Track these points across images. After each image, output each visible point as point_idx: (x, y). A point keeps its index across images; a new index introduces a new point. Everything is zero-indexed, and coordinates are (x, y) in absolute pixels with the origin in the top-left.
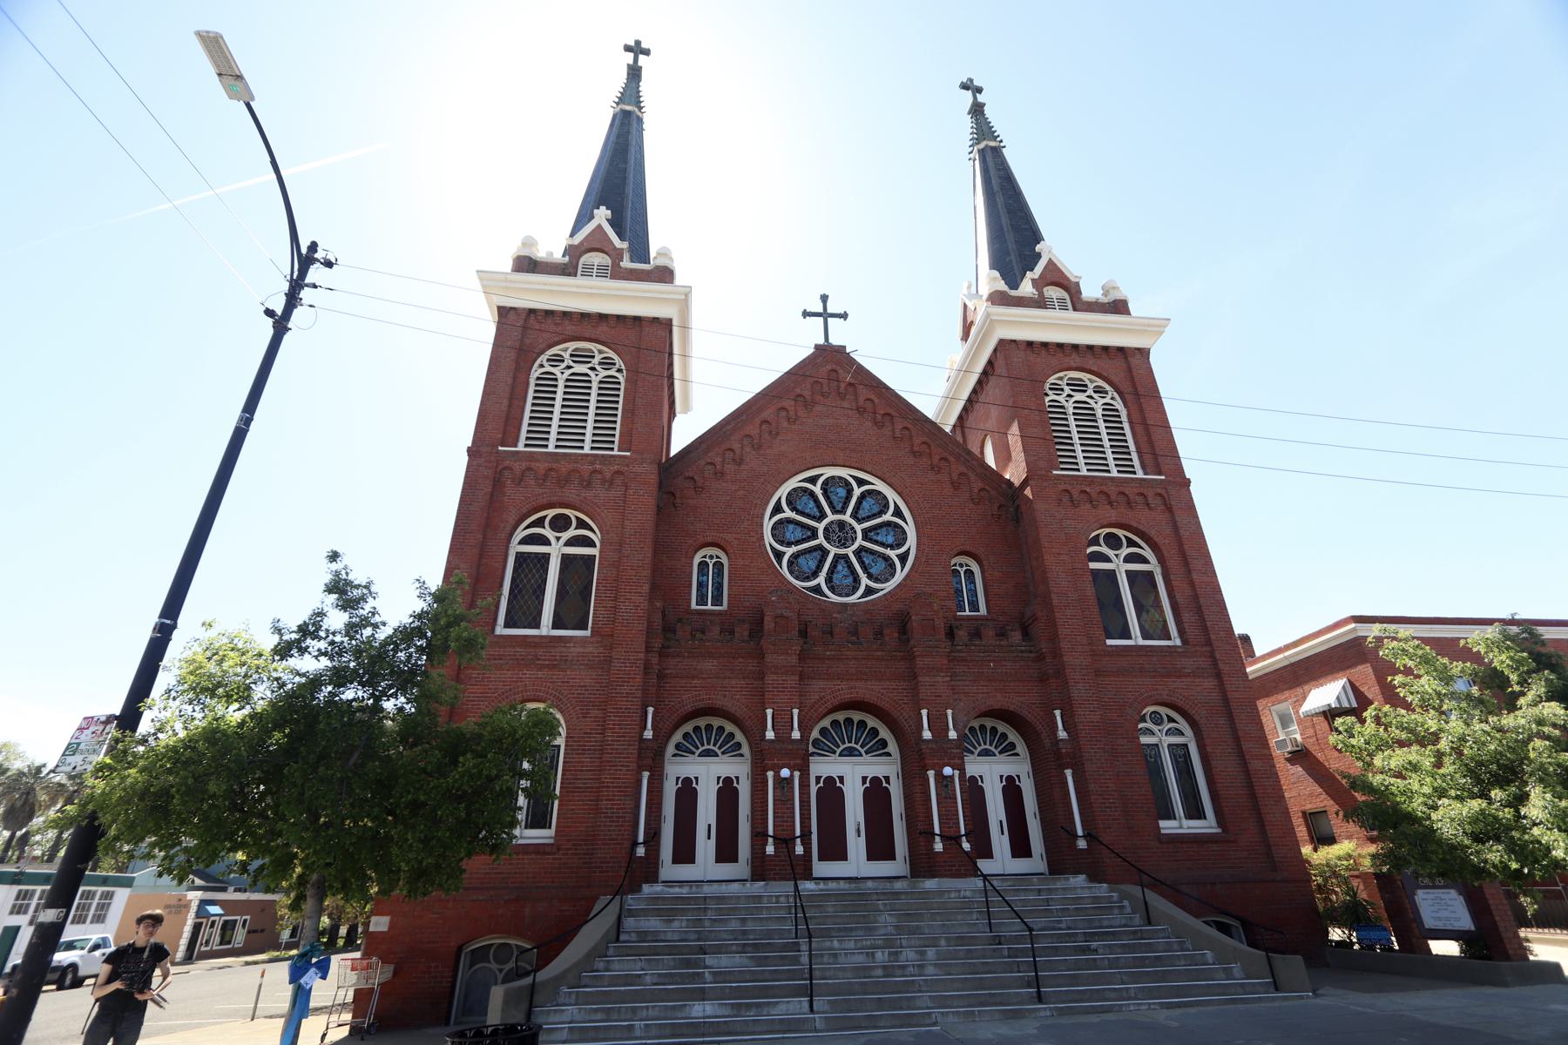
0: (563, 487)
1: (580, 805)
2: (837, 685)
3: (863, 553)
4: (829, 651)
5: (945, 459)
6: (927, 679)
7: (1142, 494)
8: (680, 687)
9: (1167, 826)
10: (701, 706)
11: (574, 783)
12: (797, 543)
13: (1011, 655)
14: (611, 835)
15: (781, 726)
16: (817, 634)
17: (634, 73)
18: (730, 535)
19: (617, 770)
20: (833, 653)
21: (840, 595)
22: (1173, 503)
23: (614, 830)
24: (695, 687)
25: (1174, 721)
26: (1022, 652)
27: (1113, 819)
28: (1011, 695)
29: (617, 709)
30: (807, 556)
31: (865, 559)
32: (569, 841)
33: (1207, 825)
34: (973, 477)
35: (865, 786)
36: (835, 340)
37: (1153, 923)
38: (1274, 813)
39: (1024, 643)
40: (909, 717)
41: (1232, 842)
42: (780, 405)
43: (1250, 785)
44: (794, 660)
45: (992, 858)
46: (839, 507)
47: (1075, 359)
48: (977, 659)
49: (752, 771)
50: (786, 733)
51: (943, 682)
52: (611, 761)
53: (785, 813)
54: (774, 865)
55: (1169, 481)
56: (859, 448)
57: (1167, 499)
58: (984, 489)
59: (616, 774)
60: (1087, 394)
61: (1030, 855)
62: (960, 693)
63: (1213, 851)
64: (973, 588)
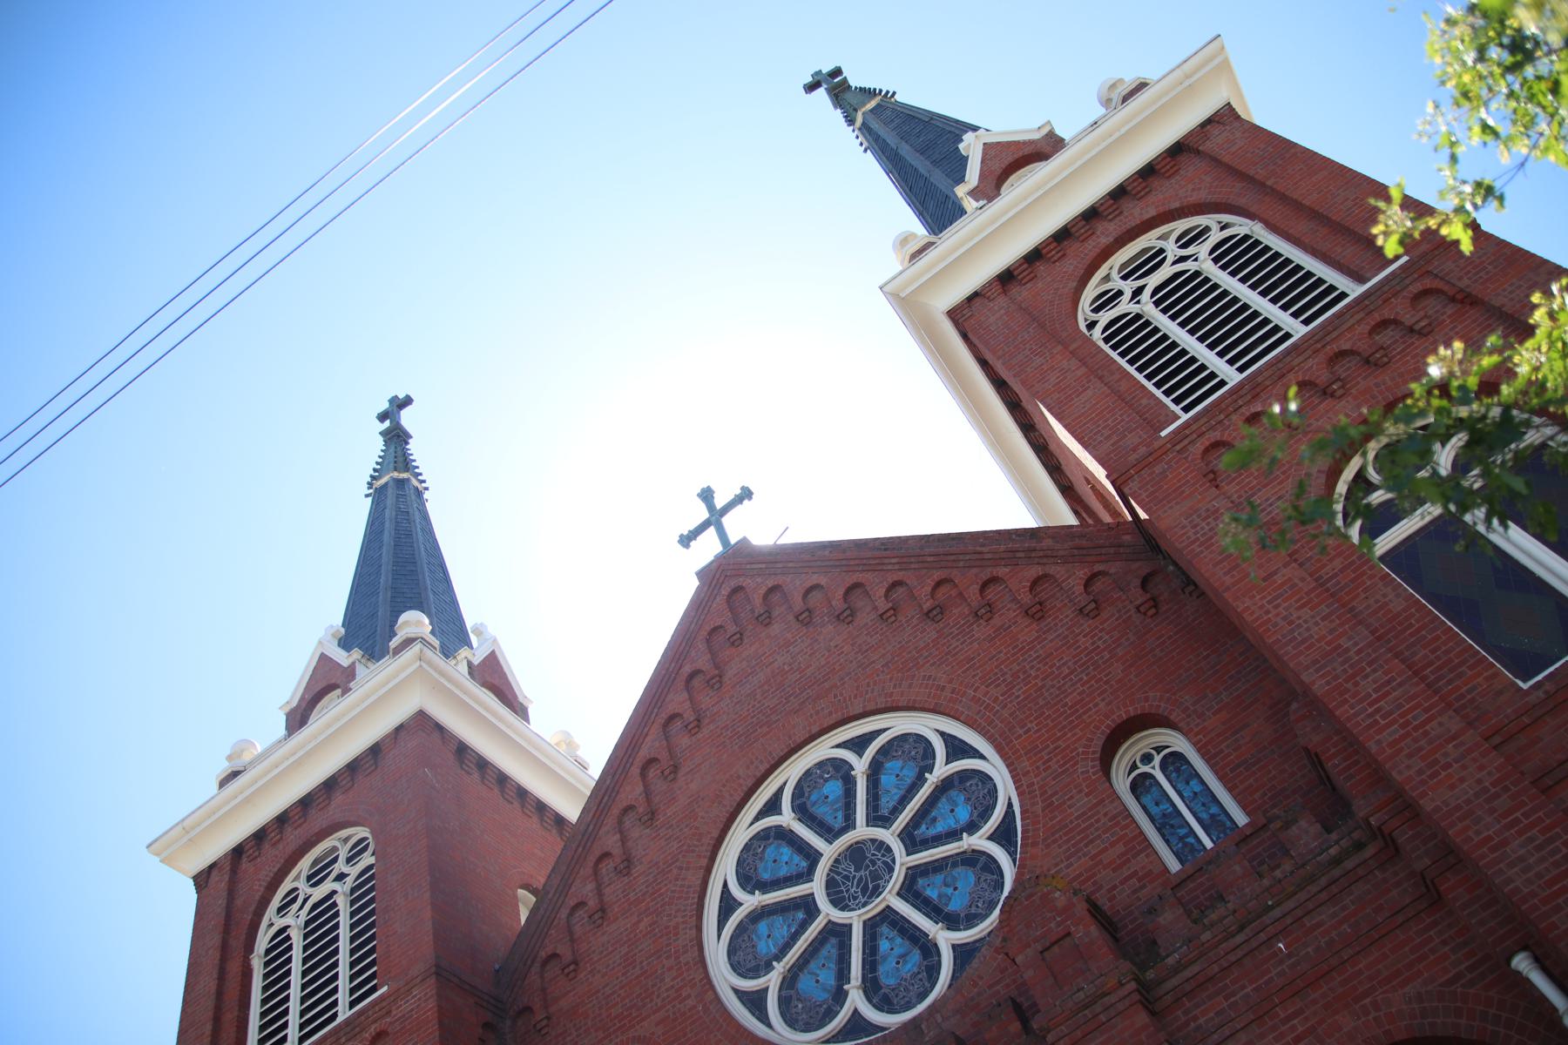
3: (921, 881)
5: (993, 580)
7: (1384, 324)
12: (843, 975)
13: (1313, 889)
17: (396, 438)
18: (645, 1024)
22: (1461, 284)
34: (1056, 570)
39: (1334, 836)
42: (664, 716)
46: (838, 823)
47: (1106, 231)
48: (1232, 958)
55: (1424, 255)
56: (827, 685)
57: (1446, 288)
64: (1198, 788)
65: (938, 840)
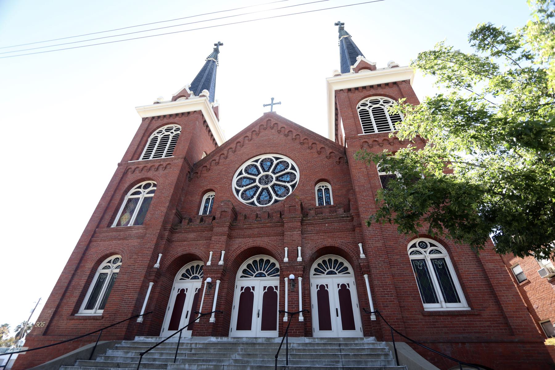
0: (148, 172)
1: (117, 297)
2: (248, 240)
3: (275, 186)
4: (245, 225)
6: (289, 233)
8: (178, 245)
9: (429, 307)
10: (185, 253)
11: (118, 287)
12: (254, 194)
14: (124, 311)
15: (215, 259)
16: (242, 218)
17: (216, 51)
19: (135, 281)
20: (247, 226)
21: (263, 204)
23: (126, 309)
24: (185, 245)
25: (434, 246)
26: (343, 217)
27: (389, 301)
28: (337, 239)
29: (143, 254)
30: (250, 190)
31: (276, 189)
32: (108, 314)
33: (462, 306)
34: (327, 148)
35: (265, 291)
36: (273, 111)
37: (400, 363)
38: (506, 296)
40: (281, 253)
41: (477, 315)
42: (245, 135)
43: (487, 279)
44: (226, 229)
45: (331, 330)
47: (373, 91)
49: (363, 326)
50: (216, 262)
51: (297, 234)
52: (134, 277)
53: (208, 301)
54: (198, 328)
58: (332, 152)
59: (134, 283)
60: (380, 104)
61: (354, 329)
62: (309, 240)
63: (463, 321)
65: (282, 181)
